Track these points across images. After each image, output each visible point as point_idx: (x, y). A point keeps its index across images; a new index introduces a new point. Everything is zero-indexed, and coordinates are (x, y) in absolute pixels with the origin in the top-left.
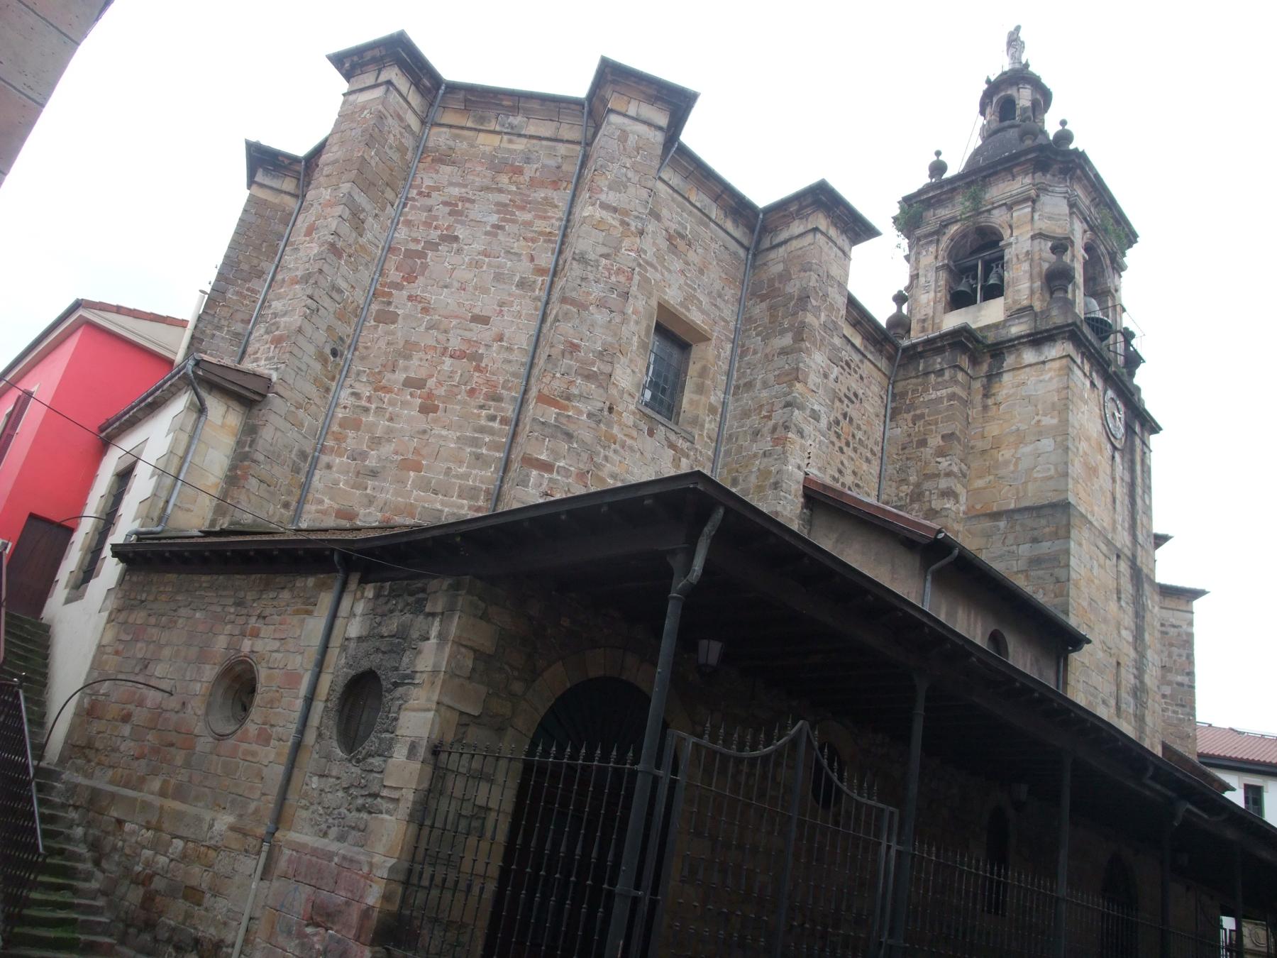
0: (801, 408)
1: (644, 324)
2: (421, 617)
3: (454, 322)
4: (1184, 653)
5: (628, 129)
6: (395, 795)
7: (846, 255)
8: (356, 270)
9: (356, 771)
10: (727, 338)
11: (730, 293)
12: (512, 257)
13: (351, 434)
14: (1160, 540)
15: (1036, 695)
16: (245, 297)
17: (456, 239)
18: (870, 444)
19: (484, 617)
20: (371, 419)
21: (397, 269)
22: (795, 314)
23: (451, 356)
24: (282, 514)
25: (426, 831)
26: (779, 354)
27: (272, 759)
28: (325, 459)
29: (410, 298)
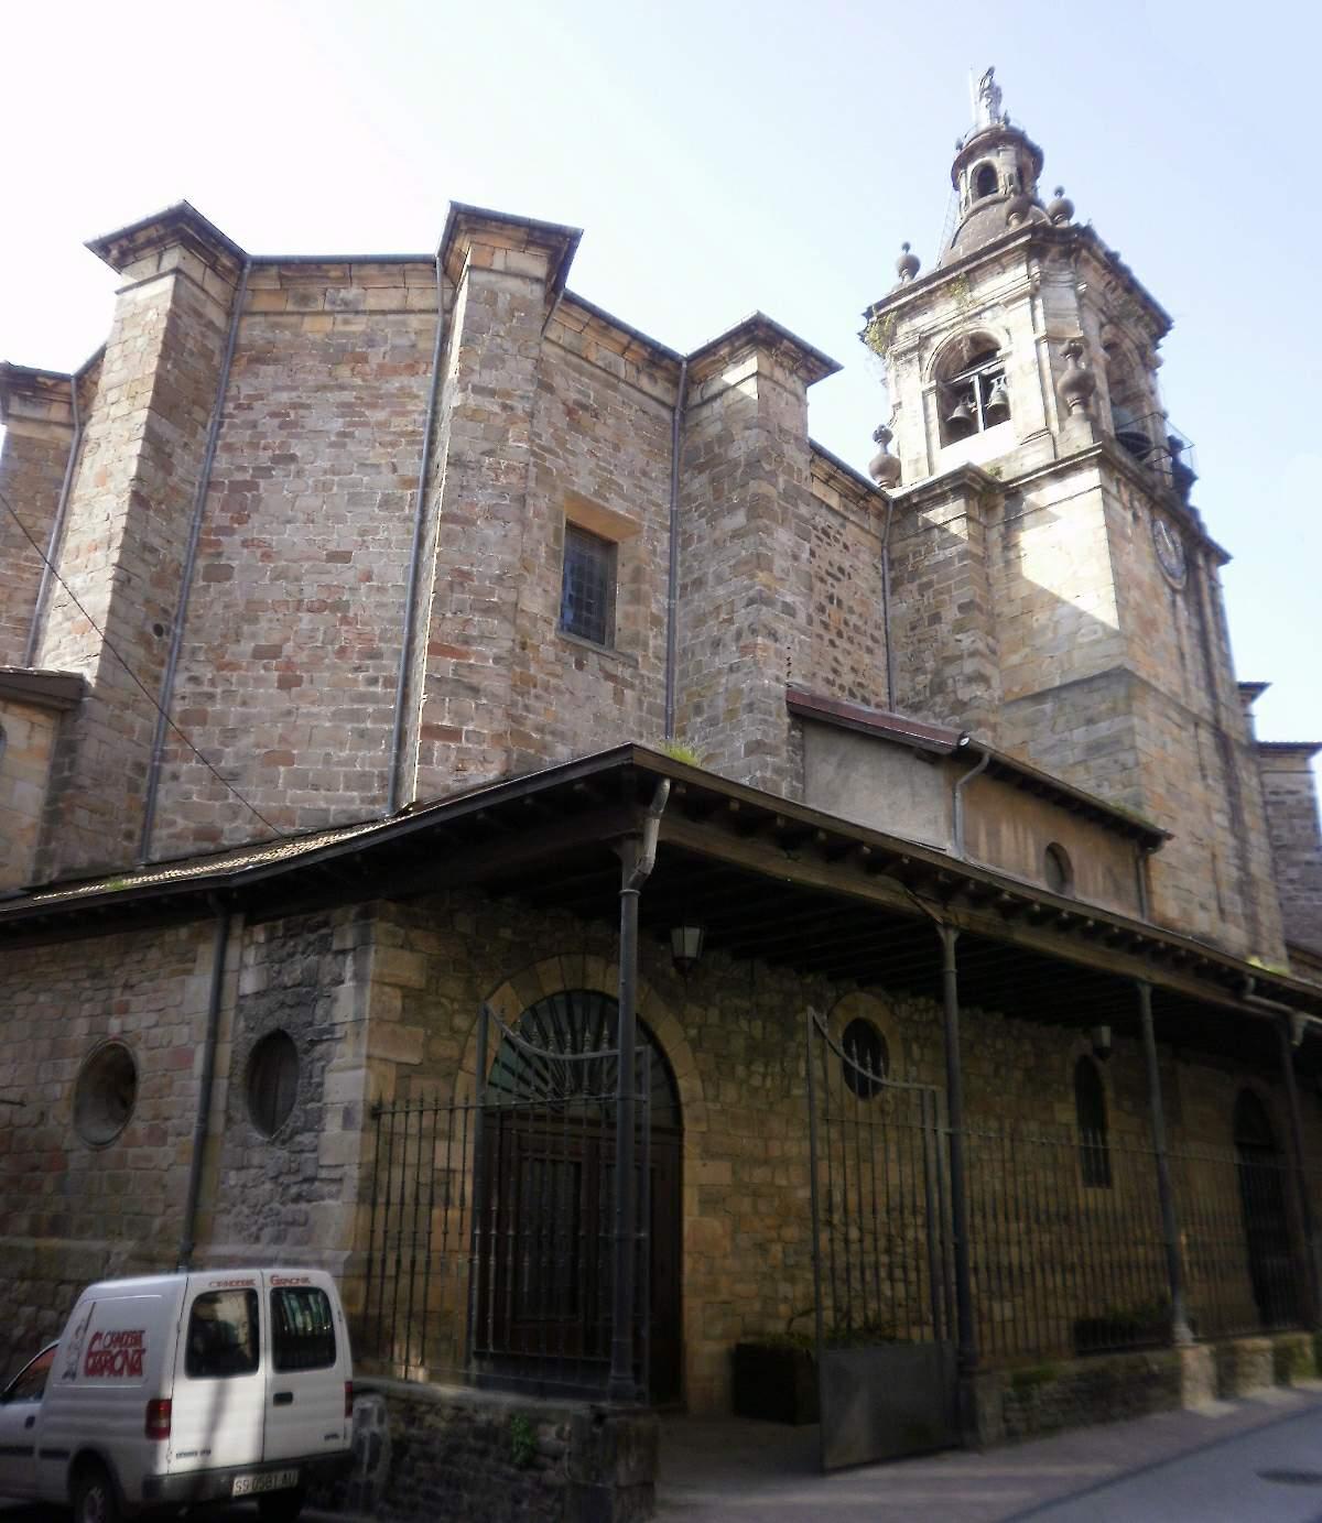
1: (551, 527)
2: (329, 957)
3: (307, 565)
4: (1309, 823)
6: (336, 1174)
7: (801, 401)
8: (170, 520)
9: (283, 1154)
10: (662, 526)
11: (658, 469)
12: (369, 470)
13: (196, 730)
14: (1253, 690)
15: (1090, 923)
16: (23, 569)
17: (293, 458)
18: (870, 630)
19: (407, 945)
20: (218, 707)
21: (222, 510)
22: (744, 485)
23: (309, 611)
24: (125, 848)
25: (381, 1211)
26: (732, 537)
27: (172, 1161)
28: (168, 768)
29: (245, 544)
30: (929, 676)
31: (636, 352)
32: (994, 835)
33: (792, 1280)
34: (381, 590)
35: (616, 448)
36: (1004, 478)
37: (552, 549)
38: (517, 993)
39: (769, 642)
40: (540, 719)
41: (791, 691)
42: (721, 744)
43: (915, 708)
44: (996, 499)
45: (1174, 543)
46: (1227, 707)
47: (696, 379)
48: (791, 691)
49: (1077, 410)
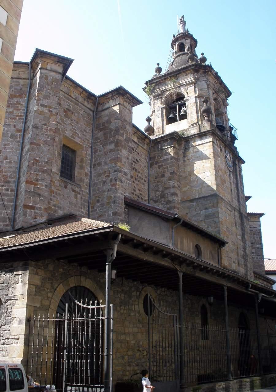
0: (121, 172)
1: (59, 146)
4: (259, 237)
5: (48, 75)
7: (131, 112)
11: (89, 129)
14: (248, 198)
15: (215, 271)
22: (114, 136)
26: (110, 152)
30: (160, 193)
31: (84, 94)
32: (182, 242)
33: (130, 366)
34: (10, 162)
35: (78, 123)
36: (186, 136)
37: (59, 152)
38: (63, 286)
39: (120, 183)
40: (55, 203)
41: (125, 198)
42: (105, 212)
43: (156, 202)
44: (180, 141)
45: (230, 157)
46: (242, 205)
47: (101, 103)
48: (125, 198)
49: (206, 118)
